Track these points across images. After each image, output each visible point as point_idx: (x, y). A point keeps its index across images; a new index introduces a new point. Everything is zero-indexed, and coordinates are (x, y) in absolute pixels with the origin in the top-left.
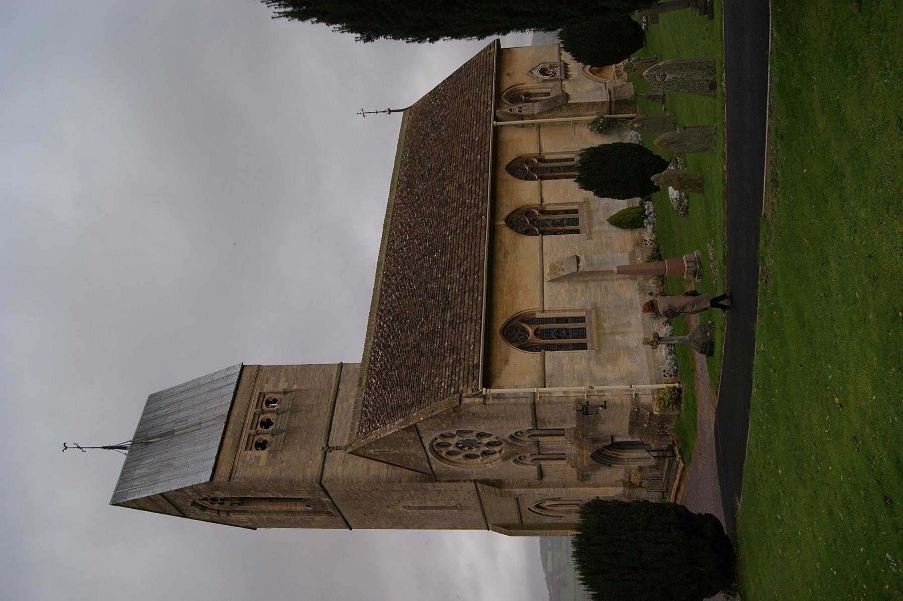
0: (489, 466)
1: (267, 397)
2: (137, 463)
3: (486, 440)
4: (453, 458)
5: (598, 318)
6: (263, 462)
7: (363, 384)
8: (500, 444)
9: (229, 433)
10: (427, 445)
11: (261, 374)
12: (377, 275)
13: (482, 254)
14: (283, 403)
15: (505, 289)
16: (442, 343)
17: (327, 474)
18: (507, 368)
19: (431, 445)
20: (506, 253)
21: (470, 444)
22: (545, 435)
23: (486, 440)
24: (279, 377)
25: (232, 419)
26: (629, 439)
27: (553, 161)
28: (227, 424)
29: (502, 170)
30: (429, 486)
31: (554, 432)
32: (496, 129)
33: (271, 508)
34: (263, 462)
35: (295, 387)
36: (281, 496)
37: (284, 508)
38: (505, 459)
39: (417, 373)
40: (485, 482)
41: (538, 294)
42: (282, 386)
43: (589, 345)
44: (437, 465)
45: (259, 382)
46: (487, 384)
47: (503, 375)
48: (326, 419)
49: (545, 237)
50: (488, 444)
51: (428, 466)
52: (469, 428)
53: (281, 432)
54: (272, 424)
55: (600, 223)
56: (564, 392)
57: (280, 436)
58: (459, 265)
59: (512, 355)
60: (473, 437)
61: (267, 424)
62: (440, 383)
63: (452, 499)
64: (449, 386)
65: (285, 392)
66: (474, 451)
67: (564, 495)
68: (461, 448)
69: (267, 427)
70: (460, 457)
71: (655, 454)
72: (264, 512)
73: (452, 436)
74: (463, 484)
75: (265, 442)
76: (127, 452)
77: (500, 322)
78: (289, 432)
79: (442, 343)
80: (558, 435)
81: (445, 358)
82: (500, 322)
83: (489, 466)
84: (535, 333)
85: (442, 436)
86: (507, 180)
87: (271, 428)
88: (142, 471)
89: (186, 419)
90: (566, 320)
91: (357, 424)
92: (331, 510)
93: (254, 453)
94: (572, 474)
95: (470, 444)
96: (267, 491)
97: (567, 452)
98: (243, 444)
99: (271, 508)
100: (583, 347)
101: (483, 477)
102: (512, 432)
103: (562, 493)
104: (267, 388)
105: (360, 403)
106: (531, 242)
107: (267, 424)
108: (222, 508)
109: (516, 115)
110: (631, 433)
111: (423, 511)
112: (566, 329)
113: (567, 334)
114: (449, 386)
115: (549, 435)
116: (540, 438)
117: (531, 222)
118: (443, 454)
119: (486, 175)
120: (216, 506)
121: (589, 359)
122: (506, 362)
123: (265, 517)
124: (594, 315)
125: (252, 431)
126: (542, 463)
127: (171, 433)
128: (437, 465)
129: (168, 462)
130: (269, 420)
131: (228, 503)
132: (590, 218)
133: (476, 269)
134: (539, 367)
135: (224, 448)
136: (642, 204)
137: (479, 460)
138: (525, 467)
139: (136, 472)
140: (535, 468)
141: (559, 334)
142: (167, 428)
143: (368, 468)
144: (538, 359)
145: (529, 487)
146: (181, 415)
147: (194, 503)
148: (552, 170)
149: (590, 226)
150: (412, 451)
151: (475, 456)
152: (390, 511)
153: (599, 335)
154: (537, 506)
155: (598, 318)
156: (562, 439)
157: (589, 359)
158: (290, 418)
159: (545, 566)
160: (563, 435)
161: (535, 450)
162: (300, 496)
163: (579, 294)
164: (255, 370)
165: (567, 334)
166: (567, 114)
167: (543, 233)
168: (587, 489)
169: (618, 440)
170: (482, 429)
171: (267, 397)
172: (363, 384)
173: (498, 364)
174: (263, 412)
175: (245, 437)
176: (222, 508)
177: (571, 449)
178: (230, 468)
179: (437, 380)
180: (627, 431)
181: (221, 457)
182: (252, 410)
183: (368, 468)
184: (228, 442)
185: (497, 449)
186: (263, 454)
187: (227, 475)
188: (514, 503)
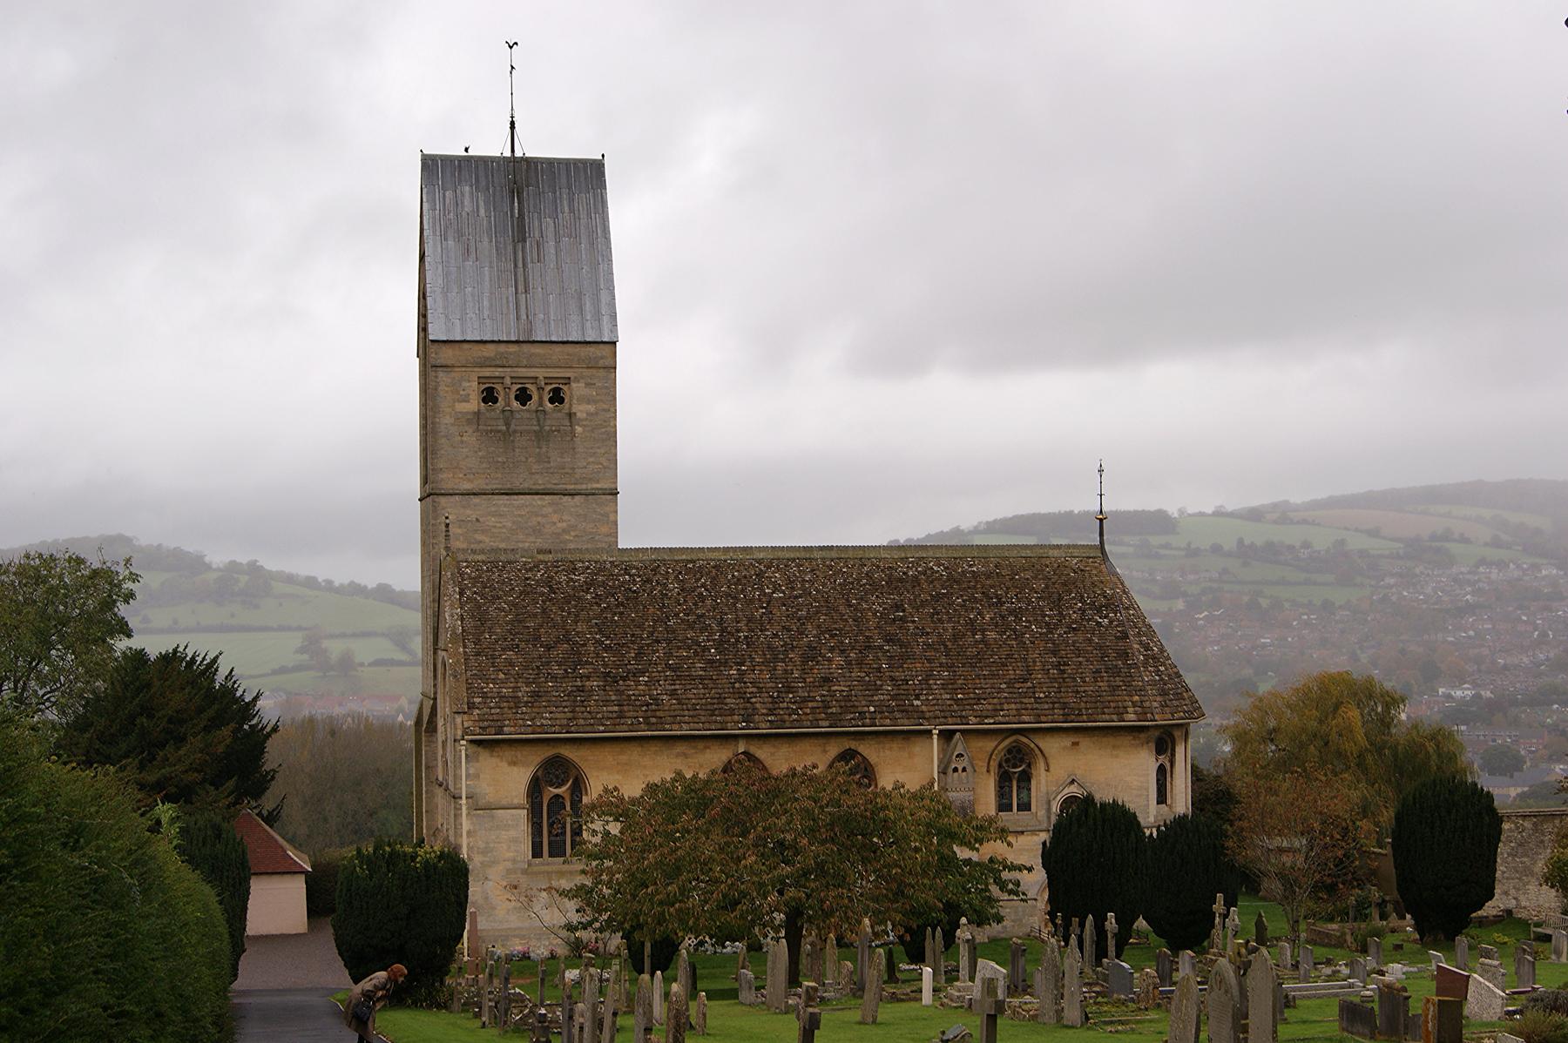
1: (565, 388)
7: (541, 557)
9: (502, 348)
11: (602, 373)
12: (727, 550)
13: (676, 727)
15: (624, 758)
16: (554, 678)
17: (443, 500)
18: (505, 764)
20: (686, 756)
24: (595, 402)
25: (525, 347)
28: (517, 342)
35: (579, 429)
42: (581, 410)
43: (537, 860)
45: (587, 372)
47: (494, 761)
54: (524, 404)
57: (501, 422)
58: (673, 693)
59: (523, 770)
61: (523, 396)
62: (494, 681)
64: (484, 696)
65: (571, 415)
69: (517, 398)
75: (495, 401)
78: (506, 437)
79: (554, 678)
81: (528, 684)
82: (568, 752)
84: (557, 796)
86: (825, 752)
91: (480, 557)
93: (473, 389)
98: (487, 372)
100: (537, 853)
105: (511, 557)
107: (523, 396)
109: (949, 762)
114: (484, 696)
119: (827, 723)
122: (513, 763)
125: (508, 381)
127: (521, 235)
129: (473, 249)
130: (530, 398)
134: (504, 802)
135: (481, 346)
139: (467, 188)
142: (532, 223)
144: (516, 801)
157: (514, 861)
158: (528, 432)
164: (608, 362)
171: (565, 388)
172: (541, 557)
173: (509, 753)
174: (540, 389)
175: (498, 372)
178: (449, 363)
179: (502, 676)
181: (466, 346)
182: (541, 373)
184: (489, 351)
186: (474, 404)
187: (438, 362)
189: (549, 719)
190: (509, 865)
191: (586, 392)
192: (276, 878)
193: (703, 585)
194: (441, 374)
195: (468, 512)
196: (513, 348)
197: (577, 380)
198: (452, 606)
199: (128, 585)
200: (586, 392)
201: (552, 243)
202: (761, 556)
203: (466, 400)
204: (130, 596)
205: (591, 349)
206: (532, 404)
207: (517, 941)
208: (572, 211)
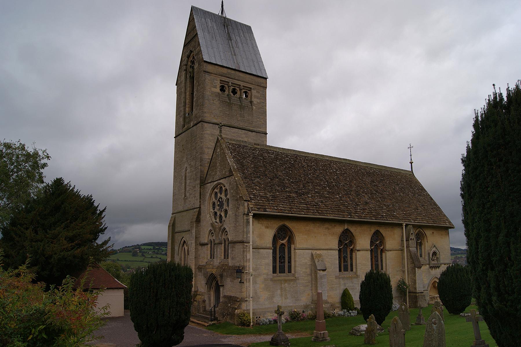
2: (214, 20)
3: (223, 214)
4: (213, 196)
6: (214, 90)
7: (256, 146)
8: (221, 222)
9: (229, 71)
10: (221, 181)
11: (262, 89)
13: (328, 215)
14: (246, 101)
16: (278, 191)
18: (263, 227)
19: (221, 184)
20: (328, 229)
22: (211, 247)
23: (223, 214)
25: (237, 72)
26: (221, 295)
27: (381, 258)
32: (401, 225)
33: (188, 94)
34: (214, 90)
35: (254, 108)
38: (212, 225)
39: (261, 177)
40: (199, 213)
42: (255, 101)
44: (210, 186)
46: (255, 216)
48: (236, 125)
50: (221, 216)
51: (209, 181)
52: (230, 205)
53: (229, 100)
54: (234, 95)
55: (345, 284)
56: (249, 260)
57: (227, 99)
58: (322, 202)
60: (225, 207)
63: (190, 194)
64: (254, 195)
65: (251, 102)
67: (190, 257)
70: (214, 199)
72: (186, 90)
73: (226, 195)
74: (199, 201)
75: (224, 91)
76: (220, 14)
78: (230, 105)
79: (278, 191)
80: (225, 255)
84: (283, 244)
85: (226, 190)
86: (370, 230)
87: (232, 94)
88: (209, 23)
90: (290, 262)
91: (234, 142)
92: (186, 127)
93: (218, 85)
94: (203, 262)
95: (221, 205)
98: (224, 79)
100: (274, 271)
101: (202, 212)
102: (227, 229)
104: (254, 92)
105: (245, 145)
106: (334, 243)
109: (409, 237)
110: (225, 297)
114: (254, 195)
115: (225, 250)
116: (223, 245)
118: (216, 190)
120: (189, 64)
122: (267, 227)
124: (293, 278)
125: (230, 84)
126: (209, 246)
127: (230, 39)
130: (236, 93)
131: (191, 70)
133: (320, 212)
134: (264, 246)
137: (212, 210)
138: (207, 236)
139: (209, 20)
140: (206, 241)
141: (282, 258)
142: (233, 36)
143: (209, 148)
144: (268, 246)
145: (196, 238)
147: (191, 52)
148: (376, 257)
149: (343, 278)
150: (218, 173)
152: (185, 159)
154: (185, 242)
156: (223, 257)
158: (237, 105)
160: (225, 258)
161: (217, 242)
165: (282, 262)
170: (230, 213)
171: (249, 92)
172: (256, 146)
173: (265, 222)
174: (240, 90)
175: (227, 80)
178: (210, 71)
181: (217, 67)
183: (209, 148)
184: (225, 71)
185: (218, 220)
186: (218, 90)
188: (187, 229)
189: (282, 208)
190: (265, 276)
191: (257, 94)
192: (116, 290)
193: (314, 165)
194: (207, 75)
195: (215, 131)
196: (233, 72)
197: (254, 89)
198: (229, 157)
199: (45, 161)
200: (257, 94)
201: (240, 44)
202: (327, 159)
203: (215, 87)
204: (45, 165)
205: (259, 79)
206: (238, 95)
207: (269, 314)
208: (244, 37)
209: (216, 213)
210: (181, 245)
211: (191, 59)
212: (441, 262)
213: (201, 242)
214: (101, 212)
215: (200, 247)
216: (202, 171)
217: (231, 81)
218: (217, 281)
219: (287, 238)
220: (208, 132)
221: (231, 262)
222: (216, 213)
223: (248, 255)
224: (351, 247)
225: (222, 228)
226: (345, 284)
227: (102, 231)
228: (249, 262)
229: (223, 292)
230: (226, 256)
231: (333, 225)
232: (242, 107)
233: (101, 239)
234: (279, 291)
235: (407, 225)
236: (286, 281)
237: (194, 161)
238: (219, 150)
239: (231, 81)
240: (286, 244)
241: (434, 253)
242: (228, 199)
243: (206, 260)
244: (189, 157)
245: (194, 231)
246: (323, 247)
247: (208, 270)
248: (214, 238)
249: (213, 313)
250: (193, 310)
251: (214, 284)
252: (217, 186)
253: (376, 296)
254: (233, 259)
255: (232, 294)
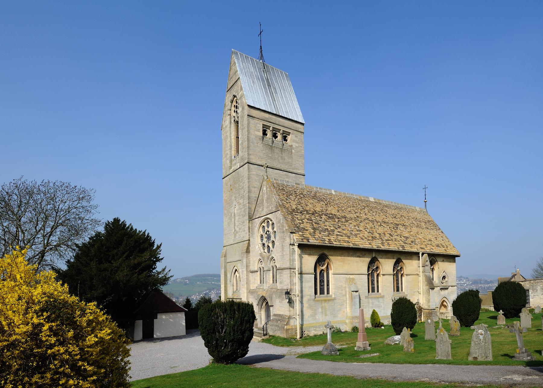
0: (257, 247)
3: (270, 245)
4: (261, 229)
5: (329, 300)
6: (257, 133)
8: (269, 252)
10: (268, 216)
19: (268, 218)
21: (269, 238)
22: (273, 274)
23: (270, 245)
26: (271, 314)
27: (402, 281)
28: (275, 115)
29: (399, 256)
30: (247, 217)
31: (275, 278)
32: (418, 253)
33: (233, 137)
34: (257, 133)
35: (293, 151)
36: (240, 142)
37: (233, 144)
38: (261, 254)
40: (249, 244)
41: (341, 272)
44: (258, 222)
45: (295, 132)
46: (300, 246)
48: (278, 167)
49: (367, 276)
50: (268, 246)
51: (257, 217)
52: (277, 237)
55: (373, 303)
56: (296, 283)
60: (272, 238)
63: (240, 229)
66: (265, 240)
67: (242, 283)
68: (266, 233)
70: (262, 233)
71: (265, 327)
72: (231, 134)
73: (273, 228)
74: (248, 234)
77: (326, 252)
78: (271, 147)
80: (273, 280)
82: (326, 252)
83: (257, 247)
84: (322, 270)
85: (273, 224)
89: (276, 93)
90: (328, 285)
92: (233, 168)
94: (253, 287)
95: (269, 238)
96: (242, 135)
97: (265, 284)
98: (266, 123)
99: (233, 137)
101: (251, 244)
102: (275, 258)
103: (243, 282)
106: (364, 269)
108: (233, 111)
110: (275, 315)
111: (233, 215)
112: (324, 285)
113: (322, 286)
115: (273, 276)
116: (271, 271)
117: (373, 270)
118: (263, 224)
120: (233, 109)
121: (310, 296)
123: (228, 134)
126: (259, 273)
128: (258, 222)
131: (234, 114)
132: (375, 298)
136: (30, 380)
137: (260, 242)
138: (256, 264)
140: (256, 269)
141: (322, 281)
143: (255, 187)
145: (247, 266)
146: (278, 91)
147: (235, 96)
148: (397, 280)
149: (372, 298)
150: (265, 209)
151: (262, 240)
152: (233, 198)
153: (322, 300)
154: (236, 270)
155: (329, 300)
156: (271, 282)
157: (310, 296)
159: (192, 277)
160: (273, 282)
161: (265, 269)
162: (240, 152)
163: (340, 292)
165: (322, 286)
166: (424, 288)
167: (368, 275)
168: (246, 294)
169: (271, 308)
170: (276, 243)
175: (269, 124)
176: (233, 111)
177: (266, 286)
178: (254, 116)
180: (276, 313)
183: (255, 187)
185: (266, 251)
188: (238, 259)
197: (292, 134)
209: (264, 244)
210: (233, 273)
211: (234, 103)
212: (449, 285)
213: (252, 270)
214: (158, 247)
215: (251, 274)
216: (249, 208)
217: (272, 125)
218: (267, 303)
219: (326, 265)
220: (254, 173)
221: (279, 286)
222: (264, 244)
223: (294, 279)
224: (378, 272)
225: (270, 257)
226: (373, 303)
227: (159, 260)
228: (296, 285)
229: (273, 311)
230: (275, 280)
231: (364, 253)
232: (282, 150)
233: (159, 266)
234: (320, 310)
235: (423, 254)
236: (325, 301)
237: (242, 199)
238: (265, 189)
239: (272, 125)
240: (325, 270)
241: (444, 277)
242: (275, 232)
243: (256, 285)
244: (237, 195)
245: (245, 261)
246: (355, 273)
247: (259, 293)
248: (263, 265)
249: (265, 329)
250: (255, 330)
251: (264, 304)
252: (264, 221)
253: (405, 314)
254: (281, 283)
255: (281, 313)
